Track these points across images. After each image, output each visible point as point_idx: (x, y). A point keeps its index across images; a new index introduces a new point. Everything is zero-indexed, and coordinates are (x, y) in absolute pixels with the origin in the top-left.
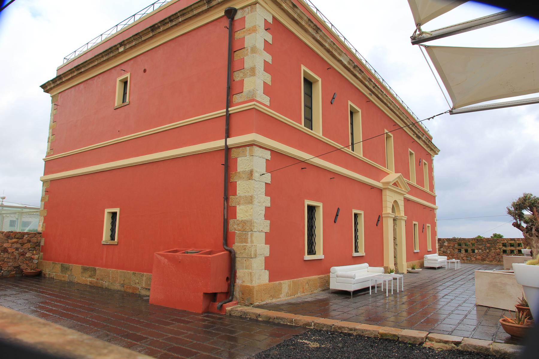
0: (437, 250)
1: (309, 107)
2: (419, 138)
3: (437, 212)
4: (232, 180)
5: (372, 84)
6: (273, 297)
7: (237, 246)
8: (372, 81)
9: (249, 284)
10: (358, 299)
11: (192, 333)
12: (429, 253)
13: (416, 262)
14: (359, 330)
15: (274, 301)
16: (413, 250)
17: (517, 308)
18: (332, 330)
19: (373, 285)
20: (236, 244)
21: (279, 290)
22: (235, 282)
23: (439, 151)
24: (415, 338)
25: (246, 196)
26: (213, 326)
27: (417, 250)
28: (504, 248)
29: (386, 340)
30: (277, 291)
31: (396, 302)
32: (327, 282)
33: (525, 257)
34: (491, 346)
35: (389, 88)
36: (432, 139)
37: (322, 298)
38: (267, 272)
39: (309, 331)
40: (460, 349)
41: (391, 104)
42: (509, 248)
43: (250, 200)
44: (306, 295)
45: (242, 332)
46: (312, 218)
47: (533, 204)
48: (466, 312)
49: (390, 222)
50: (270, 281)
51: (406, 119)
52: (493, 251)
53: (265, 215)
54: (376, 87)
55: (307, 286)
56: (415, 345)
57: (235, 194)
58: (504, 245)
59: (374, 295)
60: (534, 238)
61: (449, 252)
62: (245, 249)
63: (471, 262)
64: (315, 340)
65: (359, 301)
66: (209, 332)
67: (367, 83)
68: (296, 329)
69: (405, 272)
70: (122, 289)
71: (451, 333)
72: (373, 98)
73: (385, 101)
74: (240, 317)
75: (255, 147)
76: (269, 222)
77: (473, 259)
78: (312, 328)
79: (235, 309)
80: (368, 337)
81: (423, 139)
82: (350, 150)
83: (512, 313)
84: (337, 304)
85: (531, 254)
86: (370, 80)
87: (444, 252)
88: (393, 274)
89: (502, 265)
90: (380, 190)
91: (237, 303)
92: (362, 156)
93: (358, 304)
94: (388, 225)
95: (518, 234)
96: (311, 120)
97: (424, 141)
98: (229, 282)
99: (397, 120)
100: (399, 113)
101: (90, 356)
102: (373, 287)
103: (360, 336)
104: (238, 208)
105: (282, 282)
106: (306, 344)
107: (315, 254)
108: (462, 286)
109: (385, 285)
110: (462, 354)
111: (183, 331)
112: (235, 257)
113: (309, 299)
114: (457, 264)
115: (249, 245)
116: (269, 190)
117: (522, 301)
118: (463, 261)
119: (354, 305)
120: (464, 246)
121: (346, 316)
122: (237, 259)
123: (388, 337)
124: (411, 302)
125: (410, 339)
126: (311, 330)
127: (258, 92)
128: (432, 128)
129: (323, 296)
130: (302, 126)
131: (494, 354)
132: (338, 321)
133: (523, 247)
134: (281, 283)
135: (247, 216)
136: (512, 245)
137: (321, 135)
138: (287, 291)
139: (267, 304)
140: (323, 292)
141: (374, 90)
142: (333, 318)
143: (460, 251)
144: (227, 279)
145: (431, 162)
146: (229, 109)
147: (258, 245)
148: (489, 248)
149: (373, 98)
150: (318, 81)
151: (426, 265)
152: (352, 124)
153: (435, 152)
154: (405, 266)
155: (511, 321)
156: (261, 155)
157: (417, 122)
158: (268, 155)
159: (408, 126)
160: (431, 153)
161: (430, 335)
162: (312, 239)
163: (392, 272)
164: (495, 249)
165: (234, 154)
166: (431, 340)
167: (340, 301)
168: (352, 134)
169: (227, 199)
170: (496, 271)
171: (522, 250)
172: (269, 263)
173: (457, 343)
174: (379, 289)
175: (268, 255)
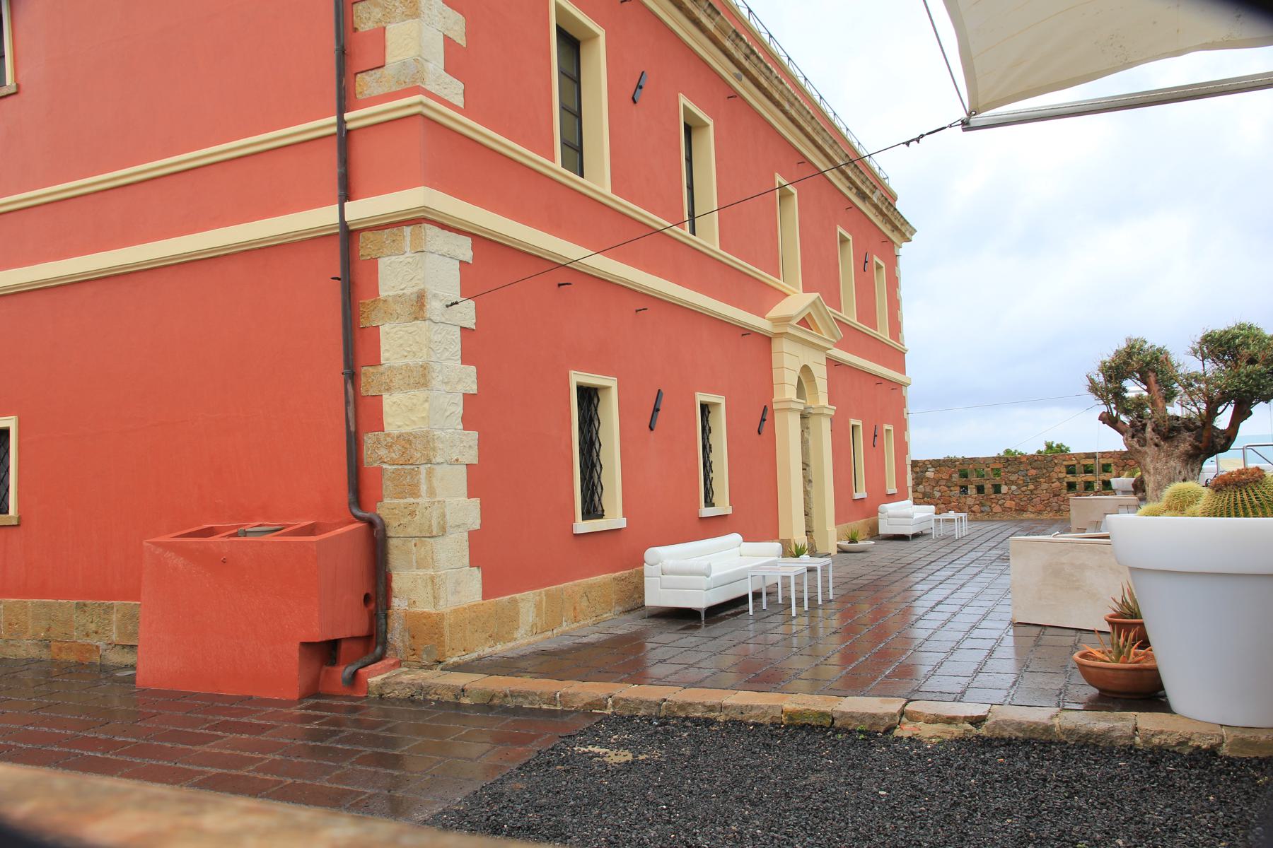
0: (910, 490)
1: (573, 113)
2: (863, 196)
3: (909, 392)
4: (364, 323)
5: (744, 46)
6: (495, 638)
7: (388, 507)
8: (742, 39)
9: (429, 609)
10: (719, 629)
11: (277, 757)
12: (891, 498)
13: (859, 524)
14: (733, 707)
15: (500, 648)
16: (851, 494)
17: (1110, 623)
18: (663, 713)
19: (756, 588)
20: (386, 501)
21: (509, 620)
22: (388, 605)
23: (913, 231)
24: (873, 716)
25: (407, 366)
26: (334, 733)
27: (861, 494)
28: (1071, 478)
29: (803, 727)
30: (505, 624)
31: (813, 628)
32: (636, 587)
33: (1119, 496)
34: (1056, 721)
35: (785, 60)
36: (895, 199)
37: (625, 631)
38: (477, 573)
39: (600, 722)
40: (985, 733)
41: (792, 105)
42: (1080, 479)
43: (421, 378)
44: (584, 626)
45: (420, 740)
46: (591, 420)
47: (1148, 364)
48: (992, 642)
49: (794, 422)
50: (486, 595)
51: (831, 147)
52: (1045, 486)
53: (464, 419)
54: (753, 57)
55: (584, 603)
56: (875, 735)
57: (376, 362)
58: (1071, 470)
59: (760, 617)
60: (1150, 450)
61: (937, 494)
62: (412, 514)
63: (990, 516)
64: (620, 745)
65: (725, 632)
66: (330, 749)
67: (728, 44)
68: (566, 719)
69: (833, 551)
70: (45, 655)
71: (959, 698)
72: (744, 89)
73: (777, 96)
74: (411, 700)
75: (427, 226)
76: (475, 435)
77: (997, 509)
78: (608, 712)
79: (393, 680)
80: (756, 725)
81: (875, 199)
82: (687, 232)
83: (1102, 636)
84: (666, 646)
85: (1139, 487)
86: (738, 35)
87: (925, 495)
88: (805, 557)
89: (1069, 520)
90: (766, 340)
91: (398, 664)
92: (717, 248)
93: (723, 642)
94: (788, 430)
95: (1114, 442)
96: (580, 150)
97: (876, 206)
98: (372, 606)
99: (809, 150)
100: (814, 129)
101: (98, 830)
102: (757, 595)
103: (737, 725)
104: (388, 401)
105: (518, 596)
106: (598, 755)
107: (601, 516)
108: (976, 579)
109: (786, 587)
110: (990, 745)
111: (247, 754)
112: (385, 538)
113: (593, 638)
114: (959, 523)
115: (423, 500)
116: (473, 346)
117: (1121, 606)
118: (974, 516)
119: (712, 645)
120: (973, 478)
121: (693, 674)
122: (393, 543)
123: (806, 721)
124: (849, 631)
125: (862, 721)
126: (607, 718)
127: (430, 66)
128: (895, 169)
129: (628, 626)
130: (555, 166)
131: (1064, 738)
132: (676, 689)
133: (1114, 473)
134: (515, 601)
135: (414, 422)
136: (1088, 470)
137: (607, 189)
138: (532, 620)
139: (480, 659)
140: (628, 617)
141: (746, 64)
142: (660, 682)
143: (964, 489)
144: (367, 599)
145: (892, 261)
146: (347, 116)
147: (447, 500)
148: (1035, 480)
149: (744, 89)
150: (596, 36)
151: (884, 529)
152: (689, 160)
153: (903, 235)
154: (831, 535)
155: (1099, 655)
156: (445, 250)
157: (861, 158)
158: (464, 248)
159: (838, 167)
160: (894, 237)
161: (911, 707)
162: (591, 477)
163: (798, 554)
164: (1050, 481)
165: (366, 247)
166: (914, 717)
167: (675, 636)
168: (691, 188)
169: (352, 376)
170: (1055, 537)
171: (1113, 480)
172: (481, 549)
173: (977, 721)
174: (772, 598)
175: (478, 527)
